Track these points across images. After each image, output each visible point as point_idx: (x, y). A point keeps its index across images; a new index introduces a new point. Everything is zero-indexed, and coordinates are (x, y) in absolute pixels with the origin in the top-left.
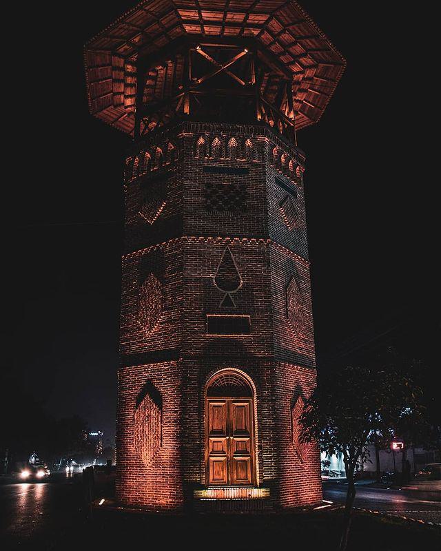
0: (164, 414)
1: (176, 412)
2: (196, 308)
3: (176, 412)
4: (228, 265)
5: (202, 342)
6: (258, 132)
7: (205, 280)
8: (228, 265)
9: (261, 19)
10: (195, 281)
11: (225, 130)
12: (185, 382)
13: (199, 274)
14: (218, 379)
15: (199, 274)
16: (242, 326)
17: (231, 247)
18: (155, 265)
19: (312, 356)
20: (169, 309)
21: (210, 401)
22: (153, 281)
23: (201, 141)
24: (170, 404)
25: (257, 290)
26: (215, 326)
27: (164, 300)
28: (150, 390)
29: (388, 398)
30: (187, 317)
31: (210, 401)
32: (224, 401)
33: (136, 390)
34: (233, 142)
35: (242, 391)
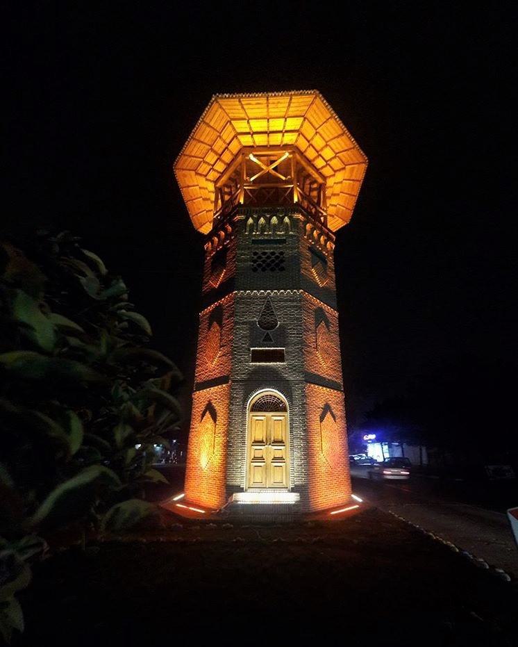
0: (217, 426)
1: (225, 425)
2: (243, 344)
3: (225, 425)
4: (268, 310)
5: (247, 369)
6: (294, 211)
7: (250, 323)
8: (268, 310)
9: (293, 124)
10: (243, 323)
11: (267, 212)
12: (231, 399)
13: (246, 318)
14: (276, 397)
15: (246, 318)
16: (279, 356)
17: (271, 298)
18: (217, 316)
19: (340, 381)
20: (224, 346)
21: (253, 416)
22: (216, 326)
23: (250, 221)
24: (221, 418)
25: (290, 329)
26: (257, 356)
27: (221, 340)
28: (210, 409)
29: (89, 283)
30: (235, 351)
31: (253, 416)
32: (265, 416)
33: (203, 408)
34: (274, 220)
35: (275, 406)
